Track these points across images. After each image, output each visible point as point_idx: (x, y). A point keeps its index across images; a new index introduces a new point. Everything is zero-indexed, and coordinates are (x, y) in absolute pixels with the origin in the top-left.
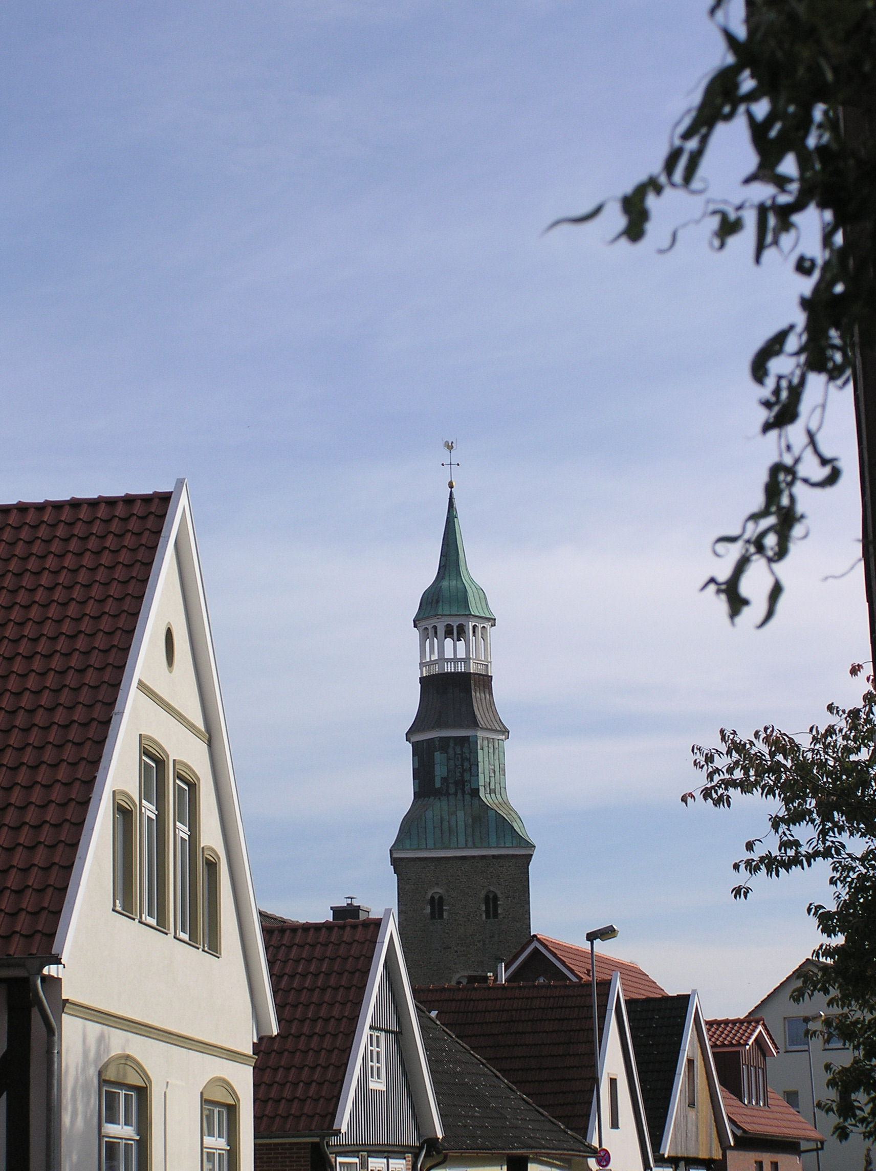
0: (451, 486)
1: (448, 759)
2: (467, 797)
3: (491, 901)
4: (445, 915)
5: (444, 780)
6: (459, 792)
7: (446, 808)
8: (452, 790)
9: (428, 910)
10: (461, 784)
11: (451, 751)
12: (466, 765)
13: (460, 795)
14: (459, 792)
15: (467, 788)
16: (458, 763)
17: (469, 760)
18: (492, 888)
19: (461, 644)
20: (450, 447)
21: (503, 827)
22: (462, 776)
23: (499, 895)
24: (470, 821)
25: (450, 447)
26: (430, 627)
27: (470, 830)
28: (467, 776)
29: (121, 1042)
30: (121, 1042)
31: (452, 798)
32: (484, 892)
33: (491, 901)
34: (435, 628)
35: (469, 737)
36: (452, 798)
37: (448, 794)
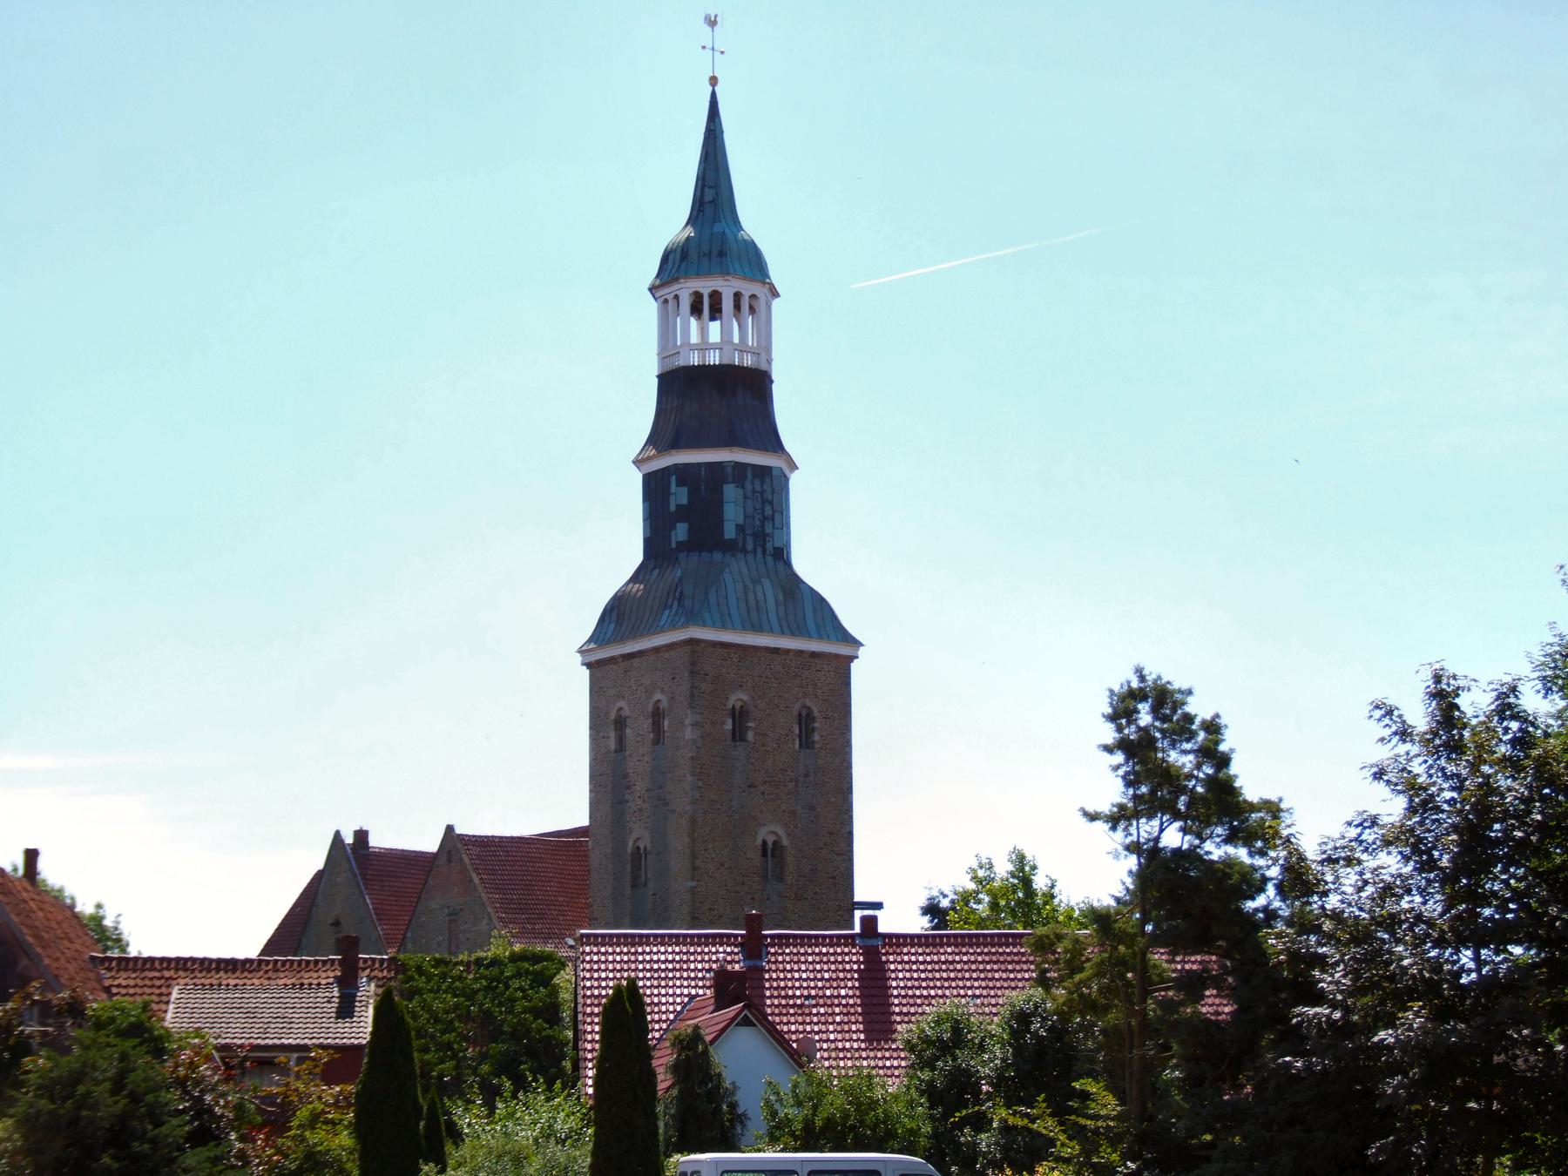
0: (714, 81)
1: (745, 497)
2: (770, 559)
3: (806, 720)
4: (750, 736)
5: (740, 528)
6: (759, 550)
7: (745, 571)
8: (750, 546)
9: (729, 726)
10: (761, 537)
11: (749, 486)
12: (768, 509)
13: (759, 554)
14: (759, 550)
15: (769, 546)
16: (758, 506)
17: (771, 503)
18: (808, 703)
19: (715, 328)
20: (712, 23)
21: (812, 612)
22: (763, 526)
23: (816, 714)
24: (781, 597)
25: (712, 23)
26: (670, 297)
27: (782, 610)
28: (769, 529)
29: (867, 912)
30: (867, 912)
31: (750, 557)
32: (797, 706)
33: (806, 720)
34: (676, 297)
35: (770, 468)
36: (750, 557)
37: (744, 551)
